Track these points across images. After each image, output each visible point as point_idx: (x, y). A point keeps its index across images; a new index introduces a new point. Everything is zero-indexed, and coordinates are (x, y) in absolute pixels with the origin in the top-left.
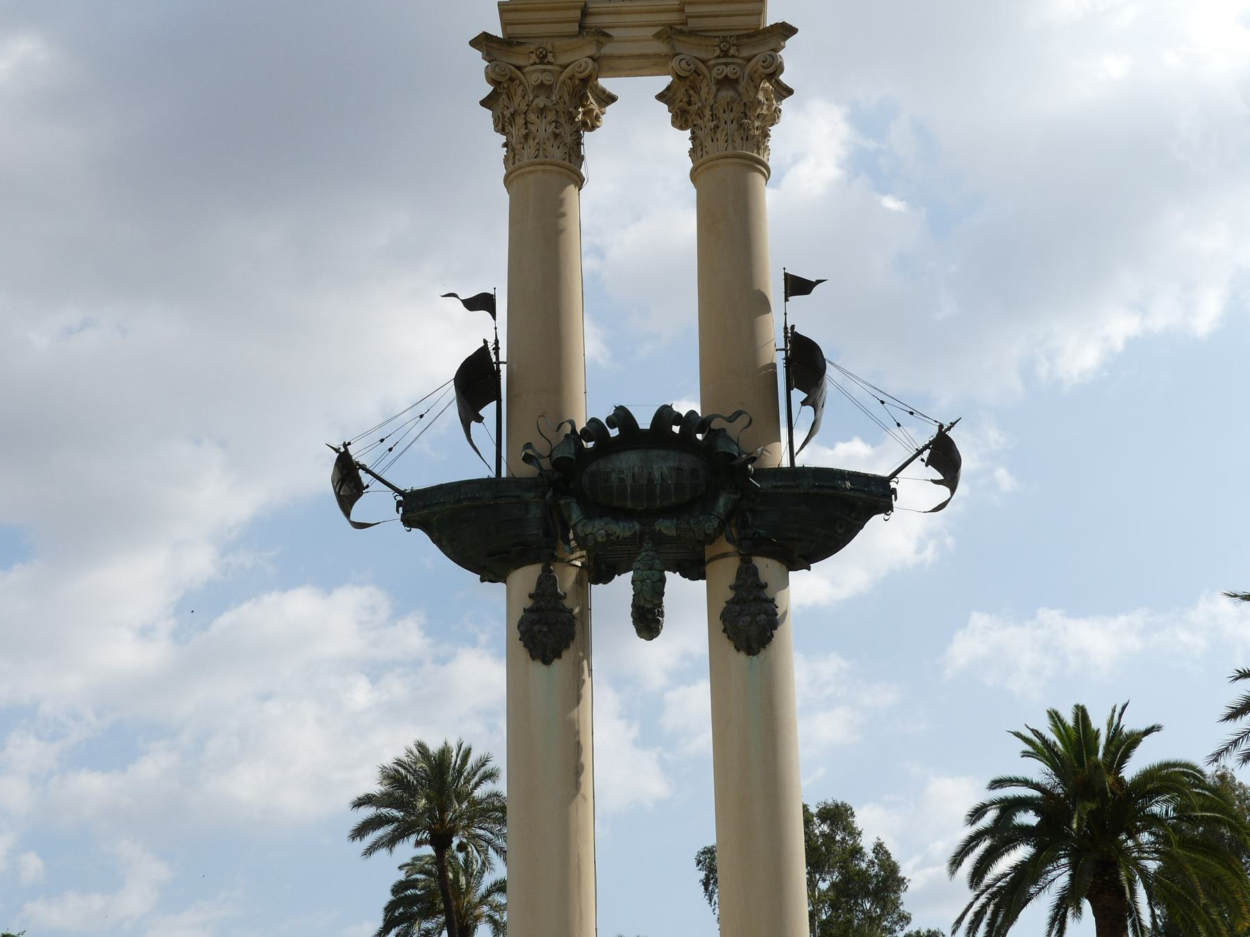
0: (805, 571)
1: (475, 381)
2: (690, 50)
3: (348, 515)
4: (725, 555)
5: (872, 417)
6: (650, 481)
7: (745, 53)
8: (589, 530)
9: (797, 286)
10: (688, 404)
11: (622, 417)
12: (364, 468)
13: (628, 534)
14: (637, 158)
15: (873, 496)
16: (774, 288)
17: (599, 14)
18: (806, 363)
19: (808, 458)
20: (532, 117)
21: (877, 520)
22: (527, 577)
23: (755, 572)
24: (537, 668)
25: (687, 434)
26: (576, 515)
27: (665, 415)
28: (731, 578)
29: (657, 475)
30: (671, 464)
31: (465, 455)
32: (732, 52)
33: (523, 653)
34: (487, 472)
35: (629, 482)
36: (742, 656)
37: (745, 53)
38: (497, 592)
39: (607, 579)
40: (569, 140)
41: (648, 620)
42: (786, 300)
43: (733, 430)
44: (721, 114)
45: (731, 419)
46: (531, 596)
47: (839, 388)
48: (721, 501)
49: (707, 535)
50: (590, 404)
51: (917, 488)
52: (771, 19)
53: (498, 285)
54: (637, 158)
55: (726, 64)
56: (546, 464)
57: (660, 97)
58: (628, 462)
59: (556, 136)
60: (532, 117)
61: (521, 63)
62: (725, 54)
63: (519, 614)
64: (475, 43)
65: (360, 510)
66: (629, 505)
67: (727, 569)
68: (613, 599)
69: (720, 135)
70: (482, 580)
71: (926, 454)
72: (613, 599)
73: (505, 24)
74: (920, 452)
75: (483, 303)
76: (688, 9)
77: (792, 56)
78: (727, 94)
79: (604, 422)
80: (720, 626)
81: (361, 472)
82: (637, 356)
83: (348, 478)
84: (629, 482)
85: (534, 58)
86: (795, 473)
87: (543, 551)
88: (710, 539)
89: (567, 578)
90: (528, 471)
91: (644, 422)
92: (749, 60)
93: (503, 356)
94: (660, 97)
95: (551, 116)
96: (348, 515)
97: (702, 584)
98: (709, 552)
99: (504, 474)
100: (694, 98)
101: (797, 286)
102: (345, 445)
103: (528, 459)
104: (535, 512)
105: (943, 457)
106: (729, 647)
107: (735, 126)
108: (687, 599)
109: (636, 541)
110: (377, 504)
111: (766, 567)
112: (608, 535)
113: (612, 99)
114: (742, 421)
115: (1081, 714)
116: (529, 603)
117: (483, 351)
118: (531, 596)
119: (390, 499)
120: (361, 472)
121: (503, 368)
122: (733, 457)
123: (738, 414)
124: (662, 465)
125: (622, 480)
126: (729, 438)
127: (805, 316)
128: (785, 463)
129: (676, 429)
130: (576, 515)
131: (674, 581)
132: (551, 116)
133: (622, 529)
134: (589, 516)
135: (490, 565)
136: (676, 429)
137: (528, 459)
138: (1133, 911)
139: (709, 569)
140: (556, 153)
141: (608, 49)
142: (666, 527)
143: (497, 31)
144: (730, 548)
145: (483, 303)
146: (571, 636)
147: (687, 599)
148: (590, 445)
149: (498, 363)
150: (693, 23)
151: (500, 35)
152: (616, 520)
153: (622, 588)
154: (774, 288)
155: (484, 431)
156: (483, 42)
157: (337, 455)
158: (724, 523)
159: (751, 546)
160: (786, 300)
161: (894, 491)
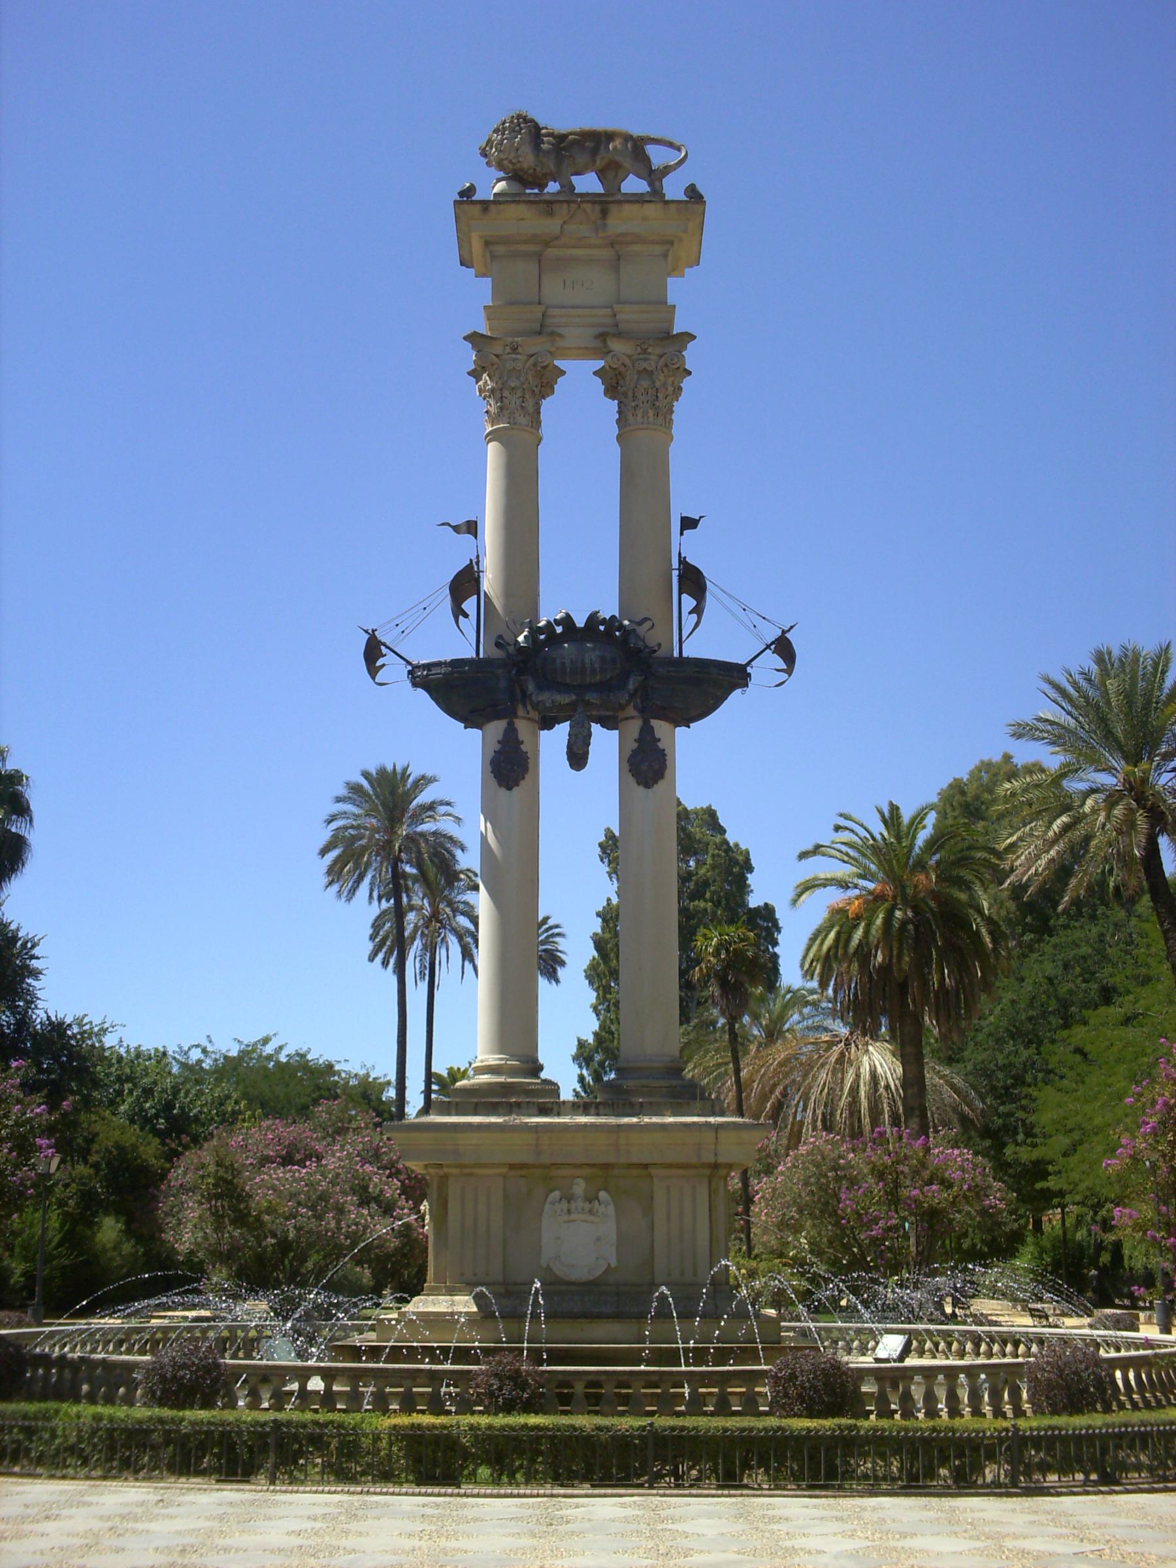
0: (684, 728)
1: (465, 583)
2: (616, 346)
3: (374, 679)
4: (633, 718)
5: (738, 619)
8: (540, 699)
9: (689, 523)
10: (609, 608)
11: (567, 621)
12: (384, 644)
13: (567, 701)
14: (579, 406)
15: (733, 676)
18: (693, 581)
19: (692, 650)
21: (738, 692)
22: (497, 727)
23: (651, 729)
24: (503, 792)
25: (609, 633)
26: (531, 687)
27: (593, 619)
28: (636, 735)
29: (587, 661)
30: (597, 653)
31: (457, 642)
32: (650, 350)
33: (493, 782)
34: (470, 654)
35: (568, 664)
36: (641, 788)
38: (476, 734)
39: (550, 727)
40: (531, 410)
41: (577, 757)
42: (682, 534)
43: (642, 630)
46: (499, 742)
47: (713, 594)
48: (631, 682)
49: (620, 705)
51: (767, 667)
54: (579, 406)
55: (645, 360)
57: (595, 373)
61: (499, 352)
63: (491, 754)
65: (381, 676)
66: (568, 681)
67: (634, 727)
68: (553, 743)
69: (639, 412)
70: (466, 728)
71: (773, 647)
72: (553, 743)
74: (768, 647)
77: (691, 356)
78: (645, 384)
80: (627, 767)
81: (383, 648)
82: (580, 584)
83: (373, 651)
84: (568, 664)
85: (508, 349)
87: (509, 714)
88: (622, 707)
89: (523, 727)
90: (497, 653)
91: (580, 622)
94: (595, 373)
95: (519, 393)
96: (374, 679)
97: (616, 732)
98: (621, 715)
99: (481, 656)
100: (621, 382)
101: (689, 523)
102: (373, 631)
104: (503, 684)
105: (784, 648)
106: (632, 781)
108: (605, 744)
109: (573, 706)
110: (393, 670)
111: (660, 727)
112: (553, 702)
113: (563, 373)
114: (647, 625)
116: (498, 747)
117: (469, 568)
118: (499, 742)
119: (404, 669)
120: (383, 648)
122: (640, 651)
123: (646, 619)
124: (592, 653)
127: (691, 547)
129: (602, 628)
130: (531, 687)
131: (596, 728)
133: (564, 699)
134: (540, 688)
135: (470, 717)
136: (602, 628)
137: (498, 645)
138: (958, 900)
139: (621, 725)
141: (560, 343)
142: (592, 697)
143: (483, 329)
144: (635, 713)
146: (525, 769)
147: (605, 744)
148: (542, 637)
151: (593, 724)
152: (559, 692)
153: (562, 730)
155: (469, 625)
156: (474, 338)
157: (367, 636)
158: (633, 695)
159: (649, 711)
160: (682, 534)
161: (749, 675)
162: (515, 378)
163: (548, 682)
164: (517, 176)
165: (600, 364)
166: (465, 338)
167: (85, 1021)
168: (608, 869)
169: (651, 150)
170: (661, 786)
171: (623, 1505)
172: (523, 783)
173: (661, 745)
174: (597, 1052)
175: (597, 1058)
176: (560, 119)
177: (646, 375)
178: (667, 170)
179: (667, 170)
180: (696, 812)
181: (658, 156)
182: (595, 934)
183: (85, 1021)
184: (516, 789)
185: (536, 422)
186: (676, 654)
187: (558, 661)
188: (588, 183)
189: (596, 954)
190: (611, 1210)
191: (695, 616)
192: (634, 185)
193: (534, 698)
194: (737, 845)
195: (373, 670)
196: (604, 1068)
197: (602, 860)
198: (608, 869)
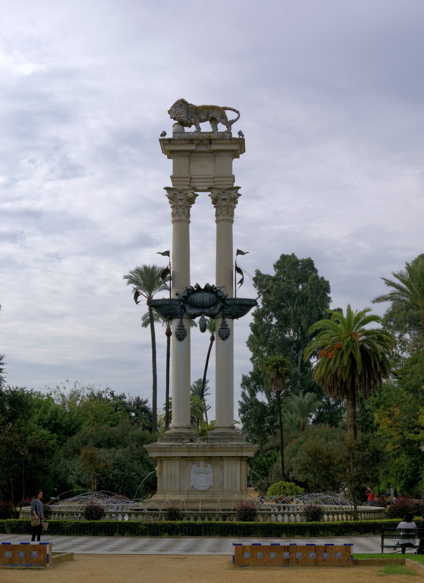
4: (219, 318)
6: (204, 301)
7: (229, 192)
9: (239, 252)
10: (213, 282)
11: (198, 286)
14: (203, 210)
16: (235, 252)
17: (194, 179)
20: (178, 207)
24: (179, 342)
29: (205, 300)
30: (208, 297)
35: (199, 301)
37: (229, 192)
43: (222, 290)
44: (223, 208)
45: (221, 288)
50: (193, 284)
52: (235, 185)
53: (169, 246)
54: (203, 210)
56: (181, 296)
57: (209, 195)
58: (198, 297)
59: (184, 212)
60: (178, 207)
62: (224, 192)
64: (165, 188)
73: (173, 185)
75: (167, 253)
76: (216, 179)
79: (193, 287)
82: (203, 272)
84: (199, 301)
86: (236, 299)
90: (176, 297)
91: (203, 287)
92: (230, 193)
93: (171, 267)
95: (183, 208)
101: (239, 252)
103: (177, 295)
107: (225, 211)
111: (228, 320)
114: (224, 288)
115: (139, 397)
121: (171, 269)
125: (197, 301)
126: (221, 292)
128: (234, 297)
132: (183, 208)
137: (177, 295)
140: (184, 217)
142: (207, 311)
145: (167, 253)
146: (186, 335)
149: (170, 268)
150: (217, 187)
154: (235, 252)
156: (167, 189)
162: (181, 199)
163: (194, 306)
164: (182, 123)
165: (218, 131)
166: (165, 188)
167: (25, 390)
168: (258, 291)
169: (227, 112)
170: (228, 340)
171: (139, 506)
172: (185, 339)
173: (228, 327)
174: (253, 381)
175: (252, 384)
176: (196, 100)
177: (226, 200)
178: (233, 122)
179: (233, 122)
180: (302, 261)
181: (230, 115)
182: (252, 324)
183: (25, 390)
184: (183, 341)
185: (188, 215)
186: (234, 297)
187: (196, 300)
188: (206, 127)
189: (252, 333)
190: (211, 470)
191: (240, 284)
192: (222, 128)
193: (188, 312)
194: (322, 278)
195: (137, 303)
196: (256, 389)
197: (255, 287)
198: (258, 291)
